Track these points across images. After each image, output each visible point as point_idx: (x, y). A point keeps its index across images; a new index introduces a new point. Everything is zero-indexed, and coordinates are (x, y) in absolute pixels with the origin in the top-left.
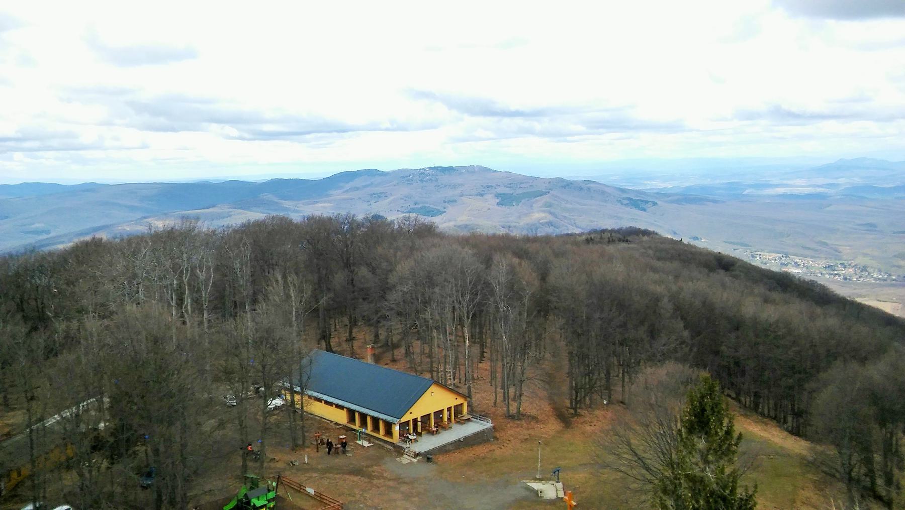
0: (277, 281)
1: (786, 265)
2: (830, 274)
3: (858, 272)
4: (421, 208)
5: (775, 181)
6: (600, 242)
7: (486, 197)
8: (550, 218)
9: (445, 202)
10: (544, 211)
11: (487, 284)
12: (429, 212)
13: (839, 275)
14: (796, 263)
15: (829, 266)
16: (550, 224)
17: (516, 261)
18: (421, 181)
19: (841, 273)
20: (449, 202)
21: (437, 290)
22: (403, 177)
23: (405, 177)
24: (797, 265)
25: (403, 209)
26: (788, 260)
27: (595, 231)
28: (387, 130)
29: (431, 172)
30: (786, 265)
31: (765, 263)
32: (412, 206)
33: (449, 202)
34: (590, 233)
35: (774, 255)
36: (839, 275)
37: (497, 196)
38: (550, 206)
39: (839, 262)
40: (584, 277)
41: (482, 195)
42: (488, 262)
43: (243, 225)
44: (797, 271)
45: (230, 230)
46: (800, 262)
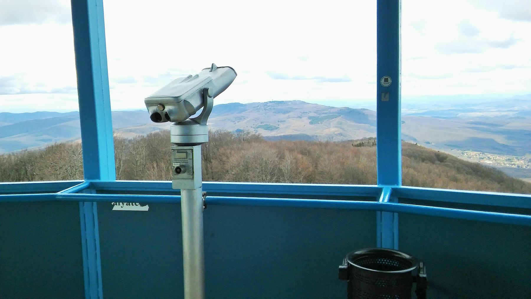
0: (154, 168)
1: (483, 158)
2: (509, 164)
3: (526, 162)
4: (265, 125)
5: (476, 108)
6: (368, 146)
7: (303, 119)
8: (341, 131)
9: (279, 122)
10: (337, 127)
11: (280, 170)
12: (269, 127)
13: (515, 165)
14: (488, 157)
15: (509, 159)
16: (341, 134)
17: (300, 156)
18: (265, 109)
19: (516, 163)
20: (281, 121)
21: (251, 173)
22: (254, 107)
23: (256, 107)
24: (489, 159)
25: (254, 126)
26: (484, 156)
27: (365, 139)
28: (18, 93)
29: (270, 104)
30: (483, 158)
31: (470, 158)
32: (260, 124)
33: (281, 121)
34: (362, 140)
35: (475, 153)
36: (515, 165)
37: (310, 118)
38: (341, 124)
39: (515, 157)
40: (338, 166)
41: (300, 118)
42: (282, 157)
43: (150, 136)
44: (489, 162)
45: (249, 135)
46: (491, 157)
